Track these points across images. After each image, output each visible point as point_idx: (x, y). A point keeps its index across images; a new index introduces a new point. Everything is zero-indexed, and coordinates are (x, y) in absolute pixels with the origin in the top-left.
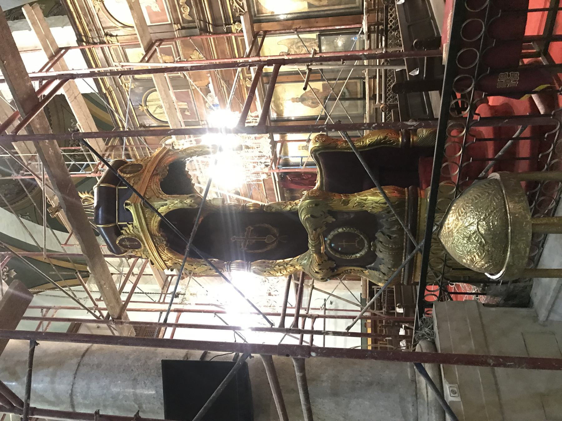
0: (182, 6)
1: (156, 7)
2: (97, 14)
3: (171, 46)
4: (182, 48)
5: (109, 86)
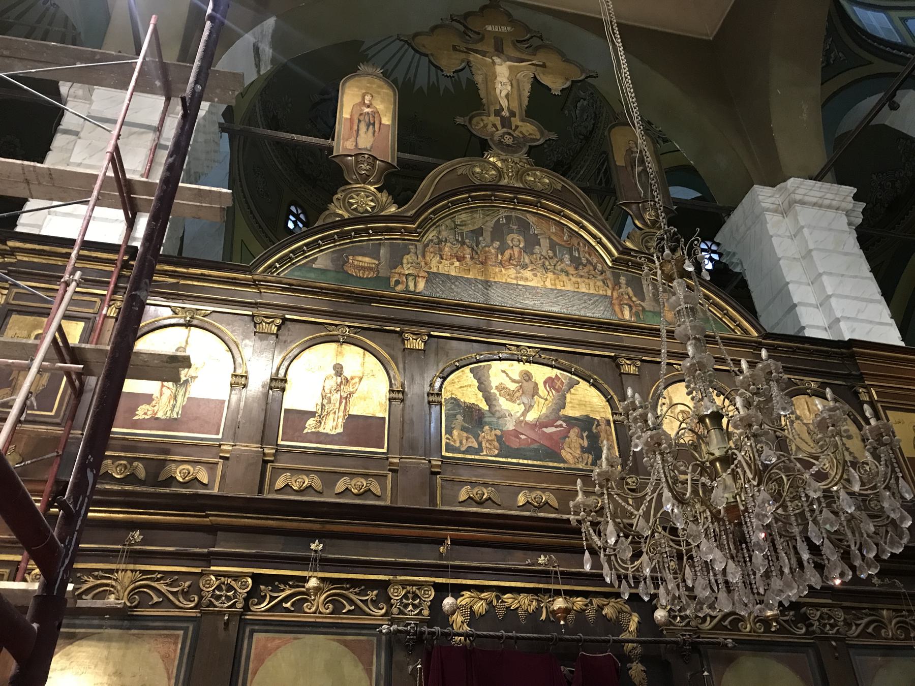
0: (131, 464)
1: (145, 414)
2: (169, 306)
3: (52, 414)
4: (39, 434)
5: (19, 258)
